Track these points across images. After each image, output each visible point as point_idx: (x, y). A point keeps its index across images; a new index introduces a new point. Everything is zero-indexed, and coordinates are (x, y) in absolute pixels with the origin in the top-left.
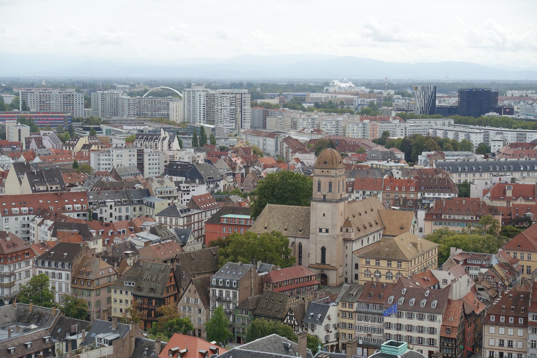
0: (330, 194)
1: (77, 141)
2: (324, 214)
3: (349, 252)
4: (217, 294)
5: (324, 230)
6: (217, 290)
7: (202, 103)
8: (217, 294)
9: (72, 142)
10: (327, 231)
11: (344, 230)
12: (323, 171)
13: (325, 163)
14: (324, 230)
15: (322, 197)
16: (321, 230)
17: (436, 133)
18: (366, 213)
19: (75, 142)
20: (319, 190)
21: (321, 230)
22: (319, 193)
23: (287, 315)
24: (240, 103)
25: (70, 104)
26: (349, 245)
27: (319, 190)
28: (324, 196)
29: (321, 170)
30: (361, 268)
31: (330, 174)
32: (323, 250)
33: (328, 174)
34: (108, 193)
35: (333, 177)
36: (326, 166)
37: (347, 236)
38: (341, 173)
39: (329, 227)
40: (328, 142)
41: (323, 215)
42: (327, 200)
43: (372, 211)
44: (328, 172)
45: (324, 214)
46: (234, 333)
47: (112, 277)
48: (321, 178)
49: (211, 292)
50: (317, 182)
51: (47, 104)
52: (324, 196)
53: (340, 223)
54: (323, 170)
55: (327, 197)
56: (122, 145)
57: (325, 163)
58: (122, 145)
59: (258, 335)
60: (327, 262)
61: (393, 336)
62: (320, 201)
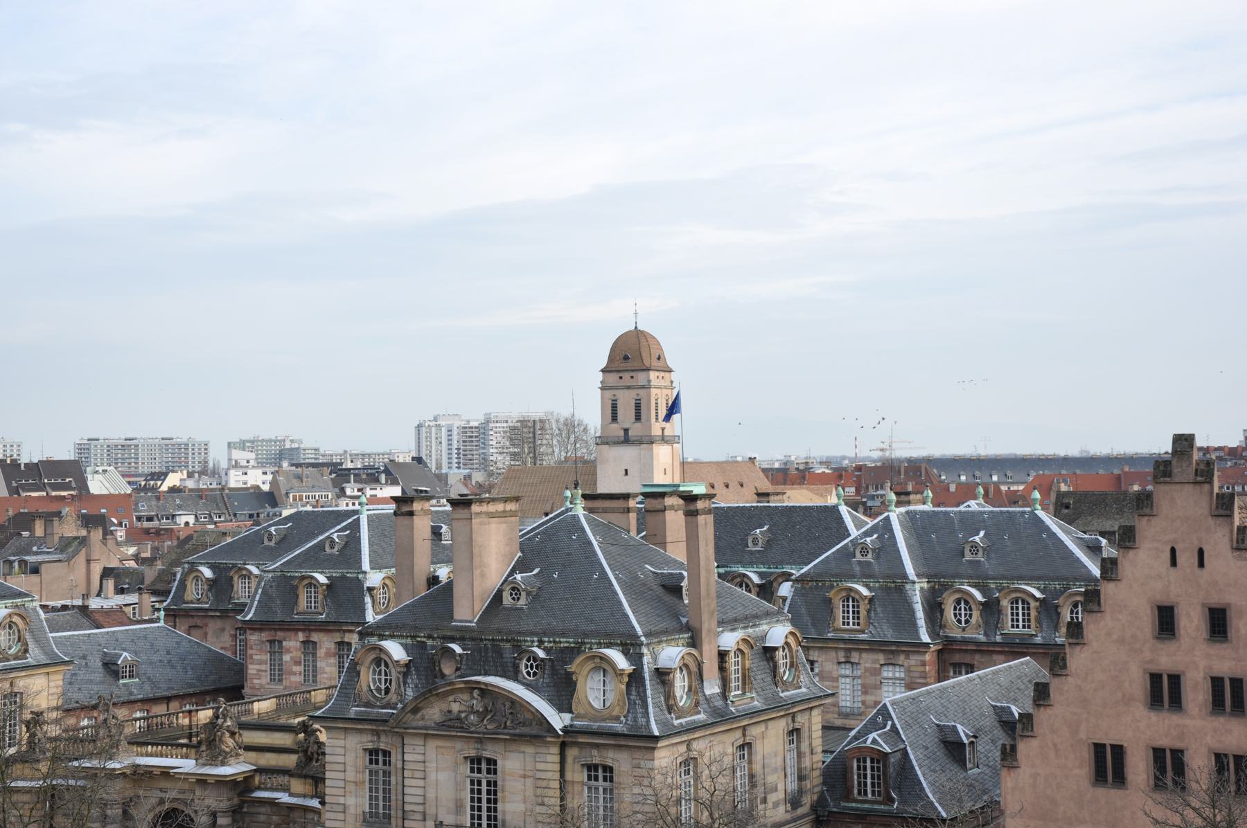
0: (638, 425)
1: (163, 480)
2: (626, 470)
7: (455, 445)
9: (152, 483)
12: (621, 378)
15: (622, 433)
18: (727, 486)
19: (159, 483)
22: (614, 425)
25: (180, 463)
28: (626, 431)
31: (637, 381)
34: (181, 499)
35: (643, 387)
36: (628, 364)
38: (663, 381)
41: (624, 472)
42: (632, 439)
43: (742, 486)
44: (632, 377)
45: (626, 470)
48: (618, 393)
50: (610, 402)
51: (130, 463)
52: (626, 431)
54: (621, 375)
55: (630, 433)
56: (248, 462)
57: (626, 358)
58: (248, 462)
59: (467, 659)
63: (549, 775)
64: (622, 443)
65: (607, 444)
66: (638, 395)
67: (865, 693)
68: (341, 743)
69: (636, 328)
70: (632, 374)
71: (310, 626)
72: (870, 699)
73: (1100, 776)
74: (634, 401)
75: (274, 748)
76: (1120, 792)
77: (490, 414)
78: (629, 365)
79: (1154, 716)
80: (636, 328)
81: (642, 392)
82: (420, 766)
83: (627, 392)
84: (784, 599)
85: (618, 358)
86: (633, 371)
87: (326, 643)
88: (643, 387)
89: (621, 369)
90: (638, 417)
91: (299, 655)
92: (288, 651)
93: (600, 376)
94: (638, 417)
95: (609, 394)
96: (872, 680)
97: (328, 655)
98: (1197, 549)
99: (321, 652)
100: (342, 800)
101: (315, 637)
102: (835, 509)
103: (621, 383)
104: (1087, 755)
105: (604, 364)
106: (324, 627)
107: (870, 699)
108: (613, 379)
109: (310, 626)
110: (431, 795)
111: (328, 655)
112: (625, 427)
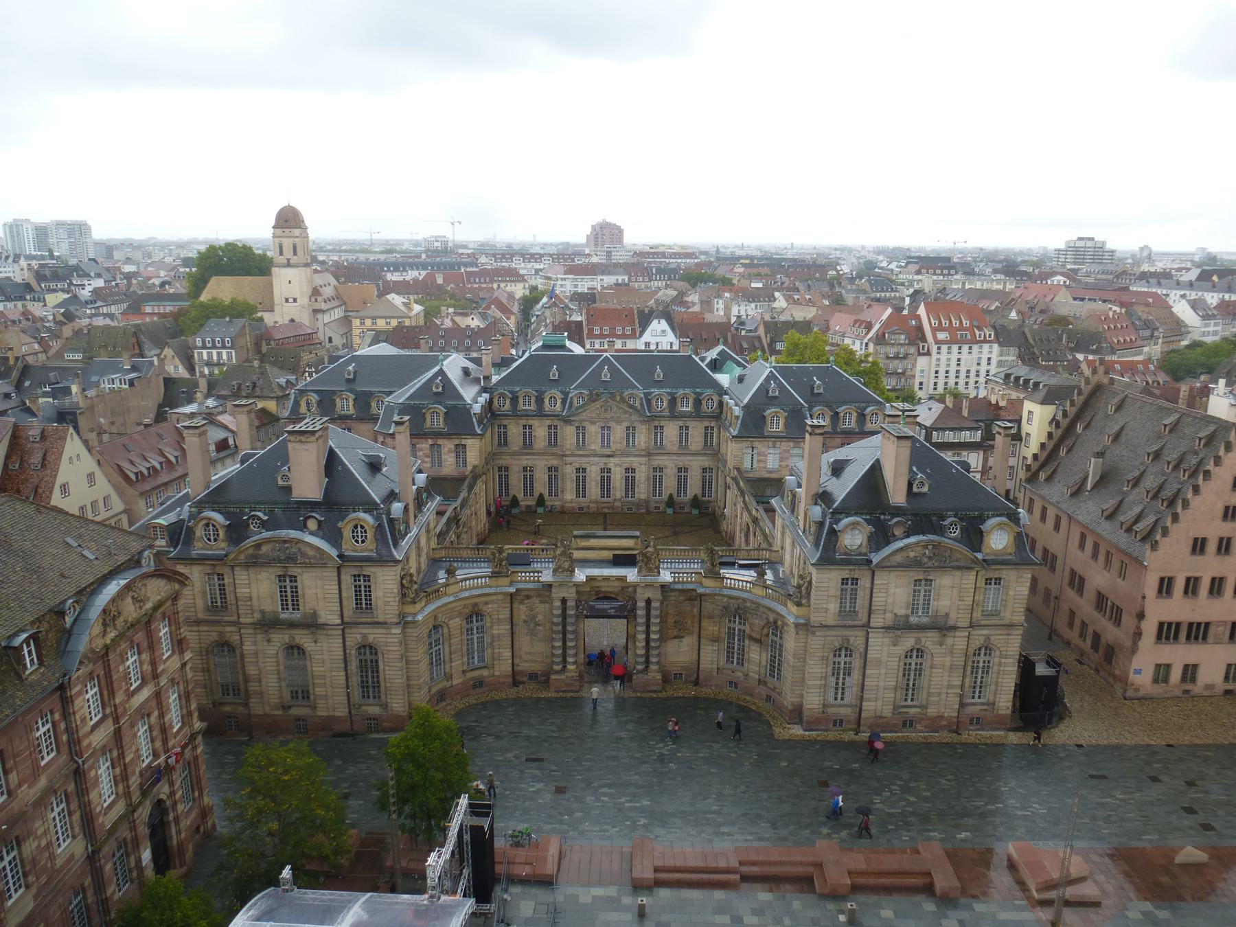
3: (320, 325)
4: (205, 357)
5: (291, 300)
6: (205, 352)
8: (205, 357)
10: (295, 300)
11: (313, 300)
13: (286, 221)
14: (291, 300)
16: (287, 300)
17: (294, 638)
21: (287, 300)
23: (305, 372)
24: (560, 628)
26: (319, 316)
27: (281, 254)
28: (288, 260)
37: (317, 306)
39: (298, 296)
46: (191, 368)
47: (40, 355)
49: (196, 355)
52: (288, 260)
53: (307, 290)
63: (968, 586)
67: (781, 461)
68: (827, 576)
71: (437, 435)
72: (784, 464)
73: (1194, 551)
76: (1202, 557)
79: (1224, 524)
82: (886, 586)
84: (737, 417)
87: (448, 445)
90: (295, 253)
91: (428, 452)
92: (421, 450)
93: (272, 231)
94: (295, 253)
95: (277, 240)
96: (786, 455)
97: (450, 451)
99: (444, 450)
100: (825, 606)
101: (440, 442)
102: (690, 356)
103: (283, 234)
104: (1191, 543)
105: (273, 223)
106: (448, 436)
107: (784, 464)
108: (279, 231)
109: (437, 435)
110: (890, 600)
111: (450, 451)
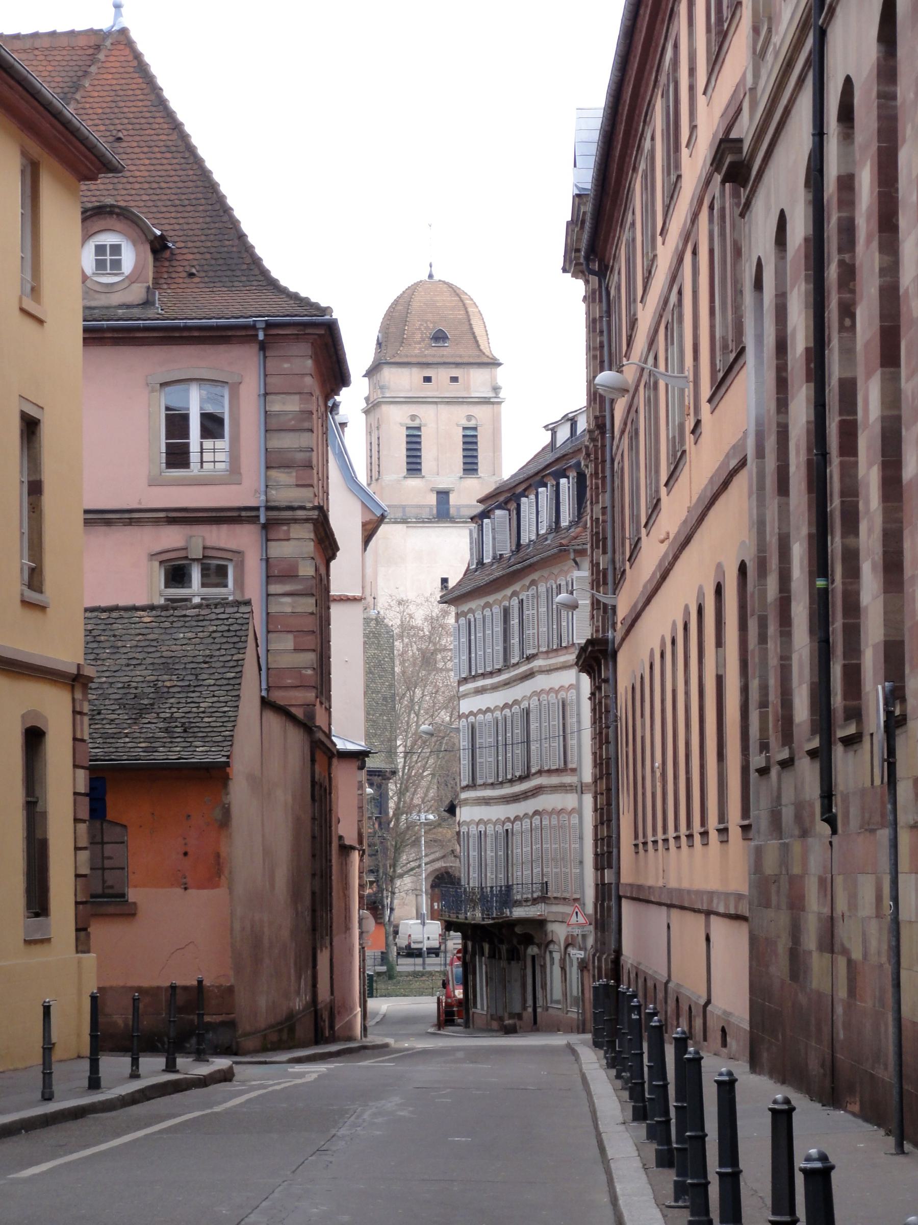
12: (428, 379)
13: (439, 337)
15: (432, 499)
20: (414, 466)
27: (414, 466)
28: (443, 495)
29: (417, 375)
30: (471, 881)
31: (467, 388)
32: (47, 1010)
33: (454, 391)
35: (486, 401)
36: (445, 352)
40: (820, 457)
44: (454, 379)
50: (404, 432)
52: (443, 495)
54: (428, 373)
55: (453, 499)
60: (550, 433)
61: (844, 418)
62: (422, 521)
64: (75, 845)
65: (404, 521)
66: (469, 418)
69: (431, 276)
70: (455, 372)
74: (460, 433)
75: (775, 145)
77: (22, 564)
78: (447, 351)
80: (431, 276)
81: (481, 413)
83: (445, 411)
85: (418, 337)
86: (457, 365)
88: (486, 401)
89: (430, 360)
98: (720, 1028)
103: (429, 391)
112: (442, 486)
